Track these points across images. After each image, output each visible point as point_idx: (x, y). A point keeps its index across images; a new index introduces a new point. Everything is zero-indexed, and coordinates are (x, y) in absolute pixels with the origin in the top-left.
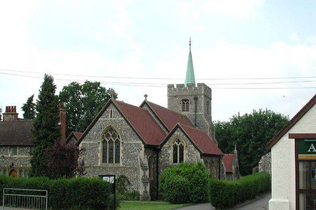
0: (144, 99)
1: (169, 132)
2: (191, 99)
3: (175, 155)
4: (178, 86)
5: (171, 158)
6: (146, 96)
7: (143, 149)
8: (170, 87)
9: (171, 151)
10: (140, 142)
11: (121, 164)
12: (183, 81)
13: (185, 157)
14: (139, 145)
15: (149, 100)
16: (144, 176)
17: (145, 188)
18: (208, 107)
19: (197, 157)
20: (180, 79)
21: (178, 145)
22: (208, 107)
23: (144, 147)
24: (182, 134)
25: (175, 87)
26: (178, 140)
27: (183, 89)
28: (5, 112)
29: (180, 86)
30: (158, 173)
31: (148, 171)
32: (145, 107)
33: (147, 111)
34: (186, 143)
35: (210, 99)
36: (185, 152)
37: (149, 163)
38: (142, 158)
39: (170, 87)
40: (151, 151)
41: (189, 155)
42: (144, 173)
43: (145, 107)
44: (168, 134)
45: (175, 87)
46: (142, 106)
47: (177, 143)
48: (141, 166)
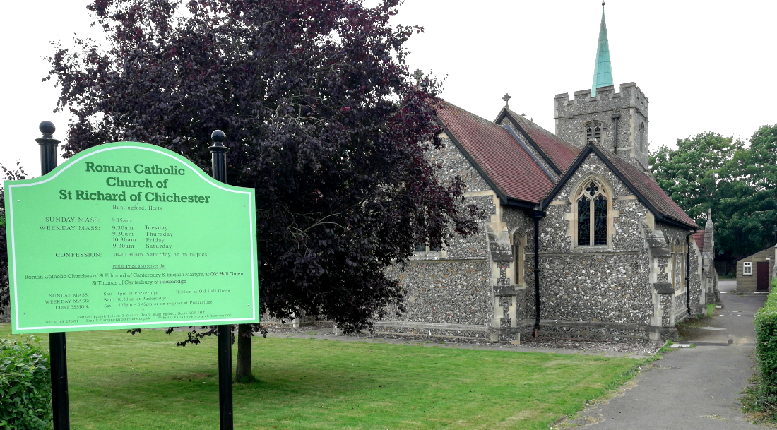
0: (503, 104)
1: (558, 173)
2: (606, 119)
3: (583, 225)
4: (577, 94)
5: (573, 233)
6: (507, 98)
7: (499, 211)
8: (560, 98)
9: (572, 216)
10: (491, 193)
11: (610, 246)
12: (587, 82)
13: (611, 230)
14: (486, 200)
15: (516, 108)
16: (503, 279)
17: (506, 311)
18: (641, 136)
19: (645, 226)
20: (583, 79)
21: (591, 198)
22: (641, 136)
23: (501, 205)
24: (603, 167)
25: (571, 98)
26: (592, 184)
27: (588, 99)
28: (526, 245)
29: (581, 95)
30: (537, 272)
31: (512, 265)
32: (506, 123)
33: (507, 131)
34: (614, 192)
35: (646, 119)
36: (612, 215)
37: (516, 247)
38: (497, 233)
39: (560, 98)
40: (519, 218)
41: (622, 224)
42: (502, 272)
43: (506, 123)
44: (556, 179)
45: (571, 98)
46: (499, 121)
47: (587, 194)
48: (494, 255)
